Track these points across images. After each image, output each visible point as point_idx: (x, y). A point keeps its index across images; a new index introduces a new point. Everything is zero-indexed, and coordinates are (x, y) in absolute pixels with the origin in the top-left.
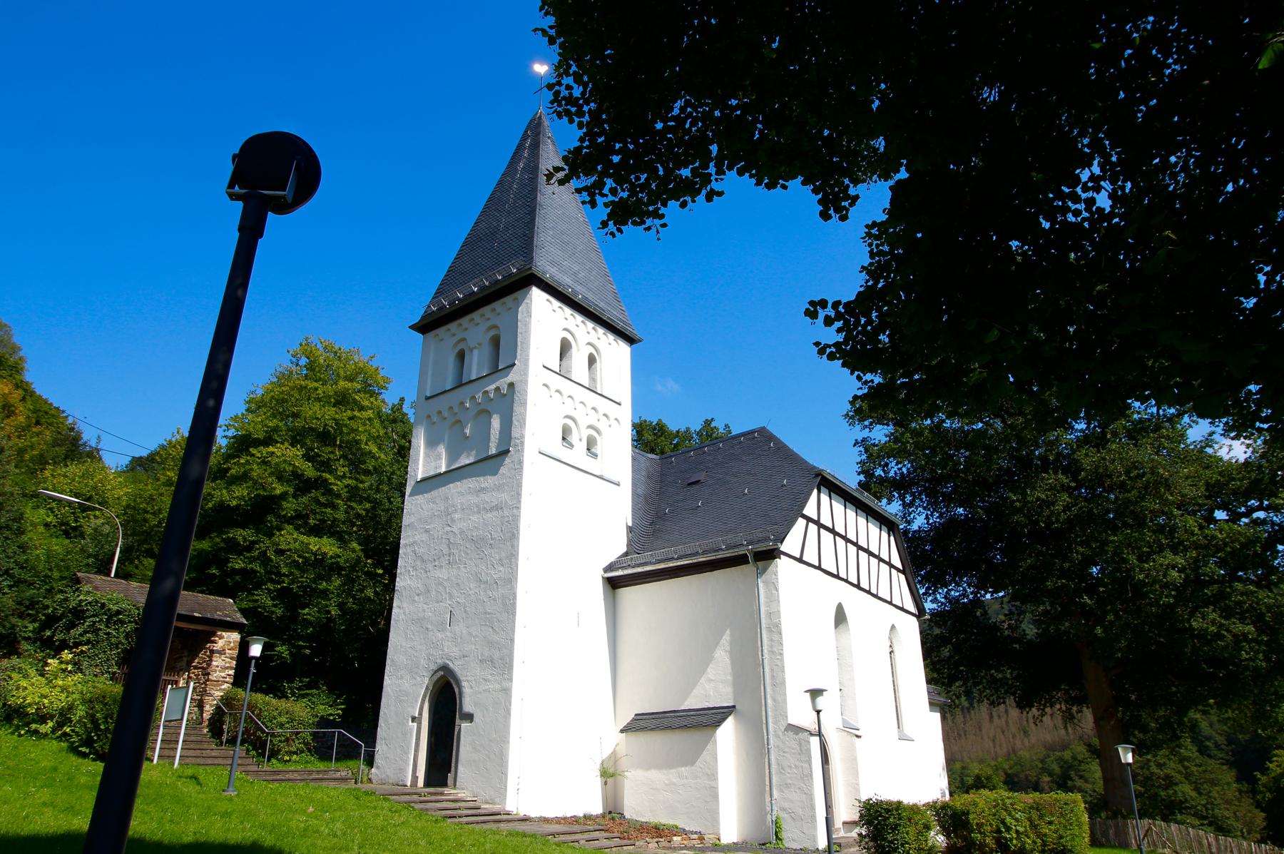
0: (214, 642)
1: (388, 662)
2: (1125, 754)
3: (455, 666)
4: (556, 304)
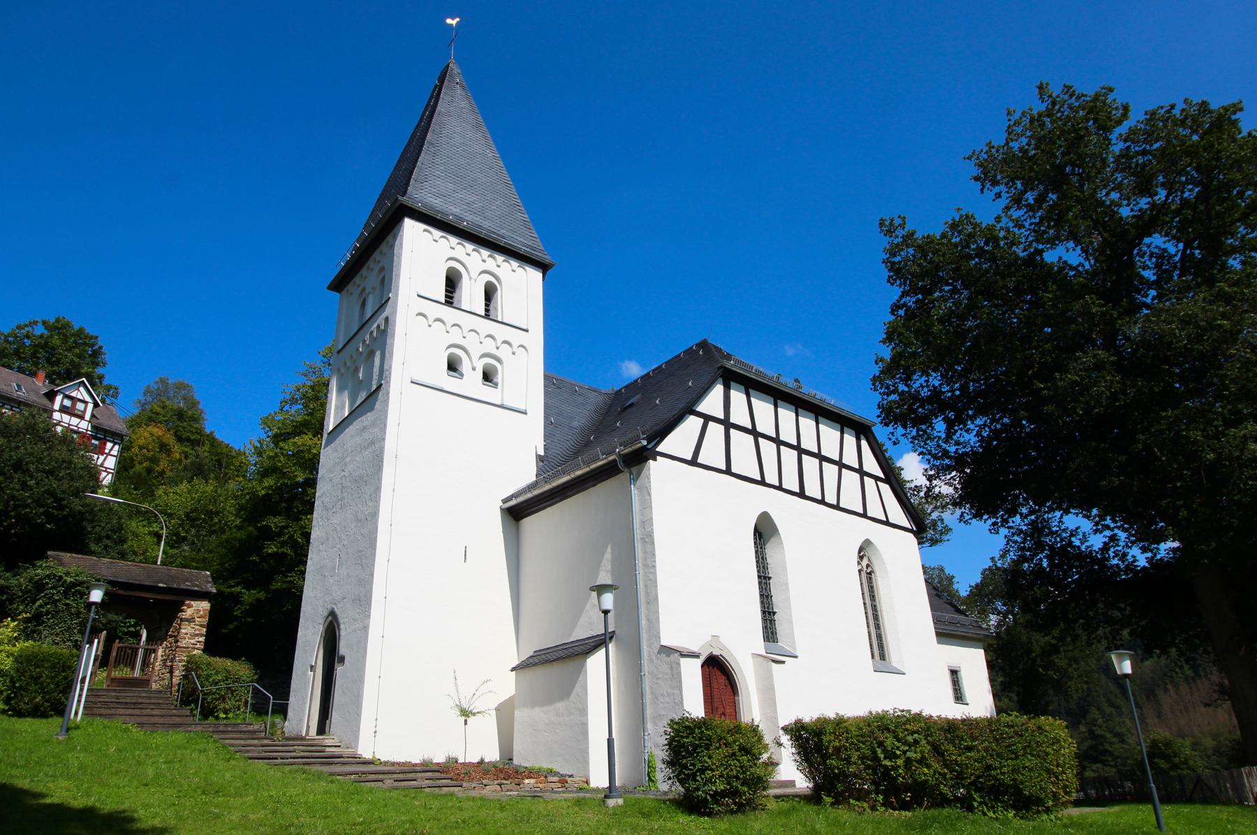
0: (183, 611)
1: (302, 614)
2: (1120, 662)
3: (336, 611)
4: (437, 233)
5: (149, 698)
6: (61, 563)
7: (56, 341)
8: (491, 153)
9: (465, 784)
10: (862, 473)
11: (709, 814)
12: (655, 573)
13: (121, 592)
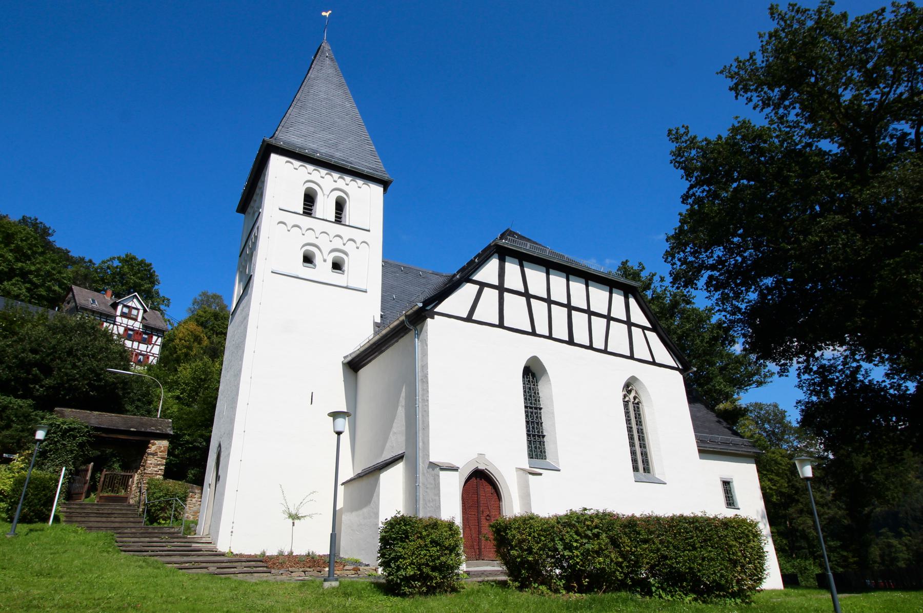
2: (802, 467)
4: (297, 163)
5: (121, 510)
6: (63, 416)
7: (126, 269)
8: (350, 105)
9: (273, 571)
10: (629, 323)
11: (404, 595)
12: (428, 406)
13: (104, 435)
